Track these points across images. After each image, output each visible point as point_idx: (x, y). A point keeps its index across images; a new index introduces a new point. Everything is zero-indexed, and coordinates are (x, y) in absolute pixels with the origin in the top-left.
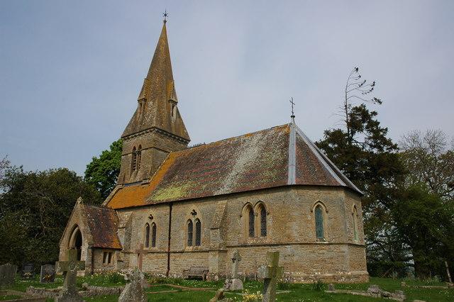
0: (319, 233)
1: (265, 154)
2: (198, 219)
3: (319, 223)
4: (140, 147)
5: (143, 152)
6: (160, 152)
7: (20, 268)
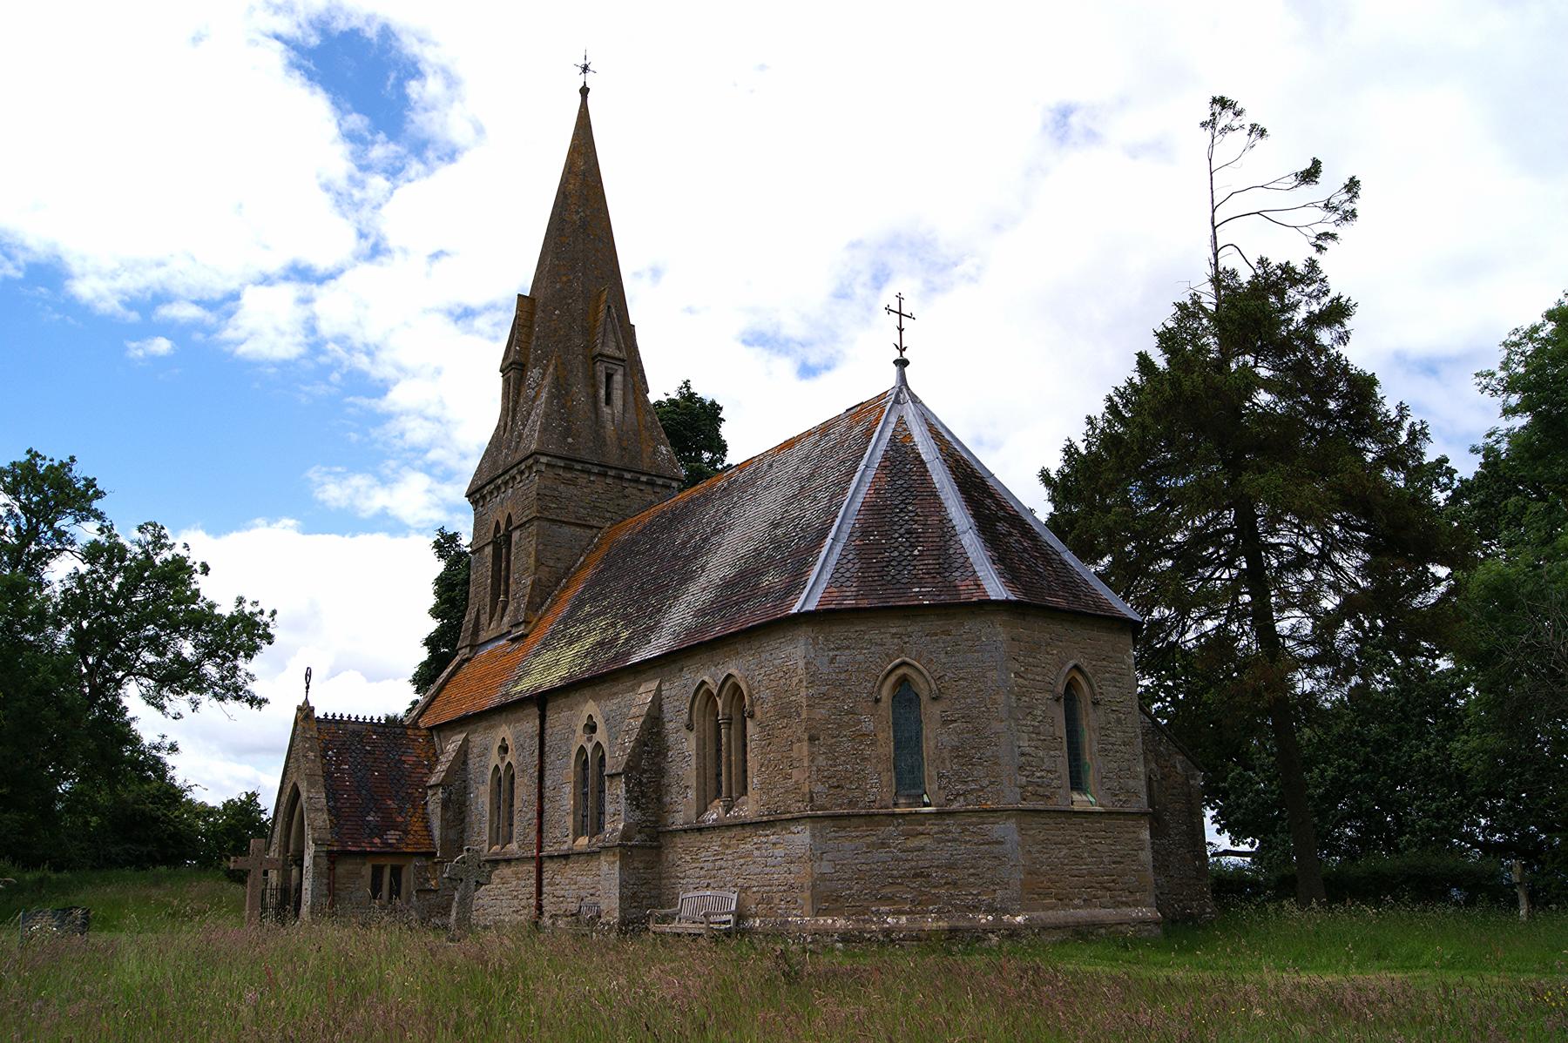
0: (908, 779)
3: (907, 743)
5: (516, 535)
6: (566, 529)
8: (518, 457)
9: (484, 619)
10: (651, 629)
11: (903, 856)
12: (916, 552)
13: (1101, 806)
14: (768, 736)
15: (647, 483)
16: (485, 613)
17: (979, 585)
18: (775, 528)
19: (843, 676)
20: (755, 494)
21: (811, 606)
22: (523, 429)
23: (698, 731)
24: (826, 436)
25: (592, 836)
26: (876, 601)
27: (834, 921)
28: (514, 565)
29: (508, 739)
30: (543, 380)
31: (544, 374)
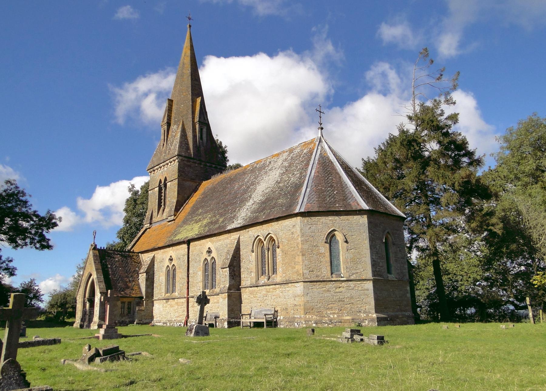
1: (285, 177)
2: (213, 258)
4: (166, 179)
7: (432, 352)
8: (169, 156)
9: (155, 214)
10: (234, 218)
11: (335, 294)
12: (335, 193)
13: (396, 278)
14: (285, 253)
15: (214, 167)
16: (155, 212)
17: (358, 204)
18: (279, 184)
19: (313, 234)
20: (266, 172)
21: (302, 210)
22: (171, 147)
23: (255, 253)
24: (292, 152)
25: (210, 290)
26: (325, 209)
27: (312, 316)
28: (168, 195)
29: (173, 256)
30: (178, 129)
31: (178, 127)
